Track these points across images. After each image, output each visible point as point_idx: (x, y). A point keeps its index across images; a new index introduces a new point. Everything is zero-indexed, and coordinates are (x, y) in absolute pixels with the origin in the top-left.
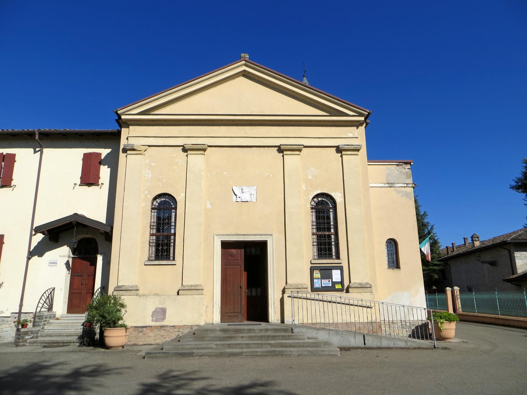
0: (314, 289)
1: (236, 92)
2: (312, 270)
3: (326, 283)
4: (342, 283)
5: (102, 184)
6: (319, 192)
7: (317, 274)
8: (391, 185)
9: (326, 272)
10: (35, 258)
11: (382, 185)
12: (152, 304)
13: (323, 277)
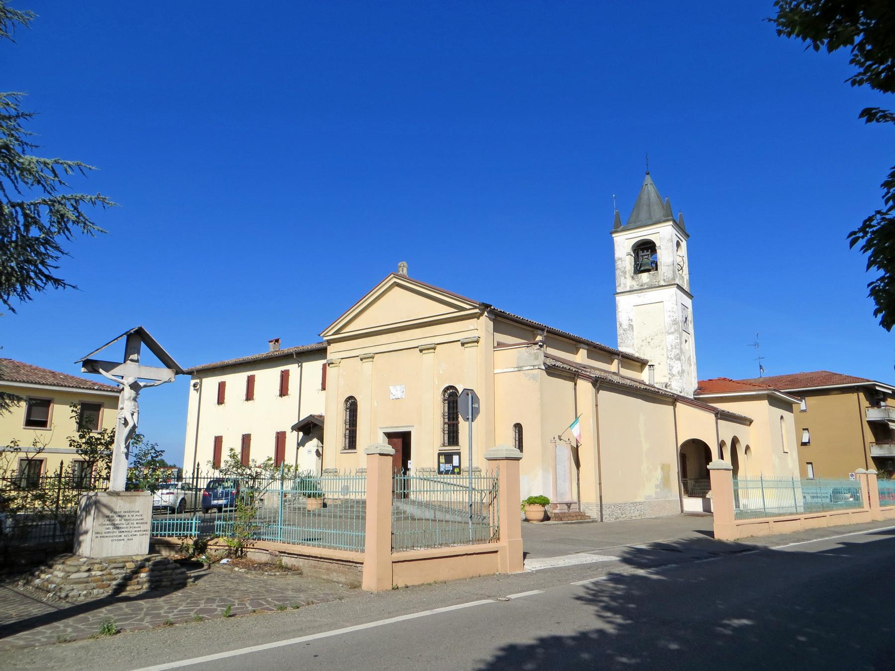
0: (440, 473)
1: (397, 304)
2: (439, 454)
3: (449, 467)
4: (459, 467)
5: (122, 409)
6: (447, 385)
7: (442, 460)
8: (520, 369)
9: (448, 457)
10: (301, 448)
11: (512, 370)
12: (340, 484)
13: (446, 462)
